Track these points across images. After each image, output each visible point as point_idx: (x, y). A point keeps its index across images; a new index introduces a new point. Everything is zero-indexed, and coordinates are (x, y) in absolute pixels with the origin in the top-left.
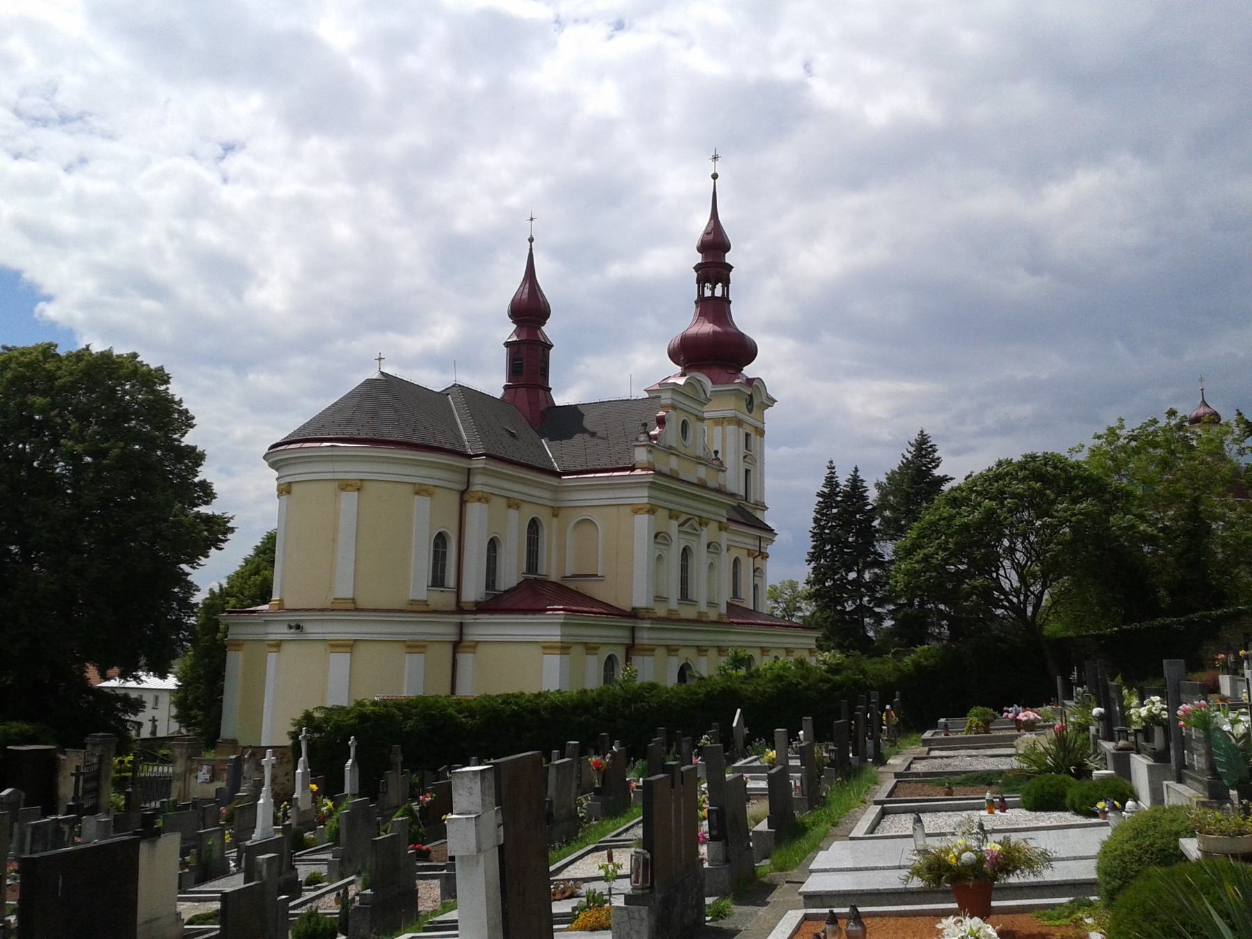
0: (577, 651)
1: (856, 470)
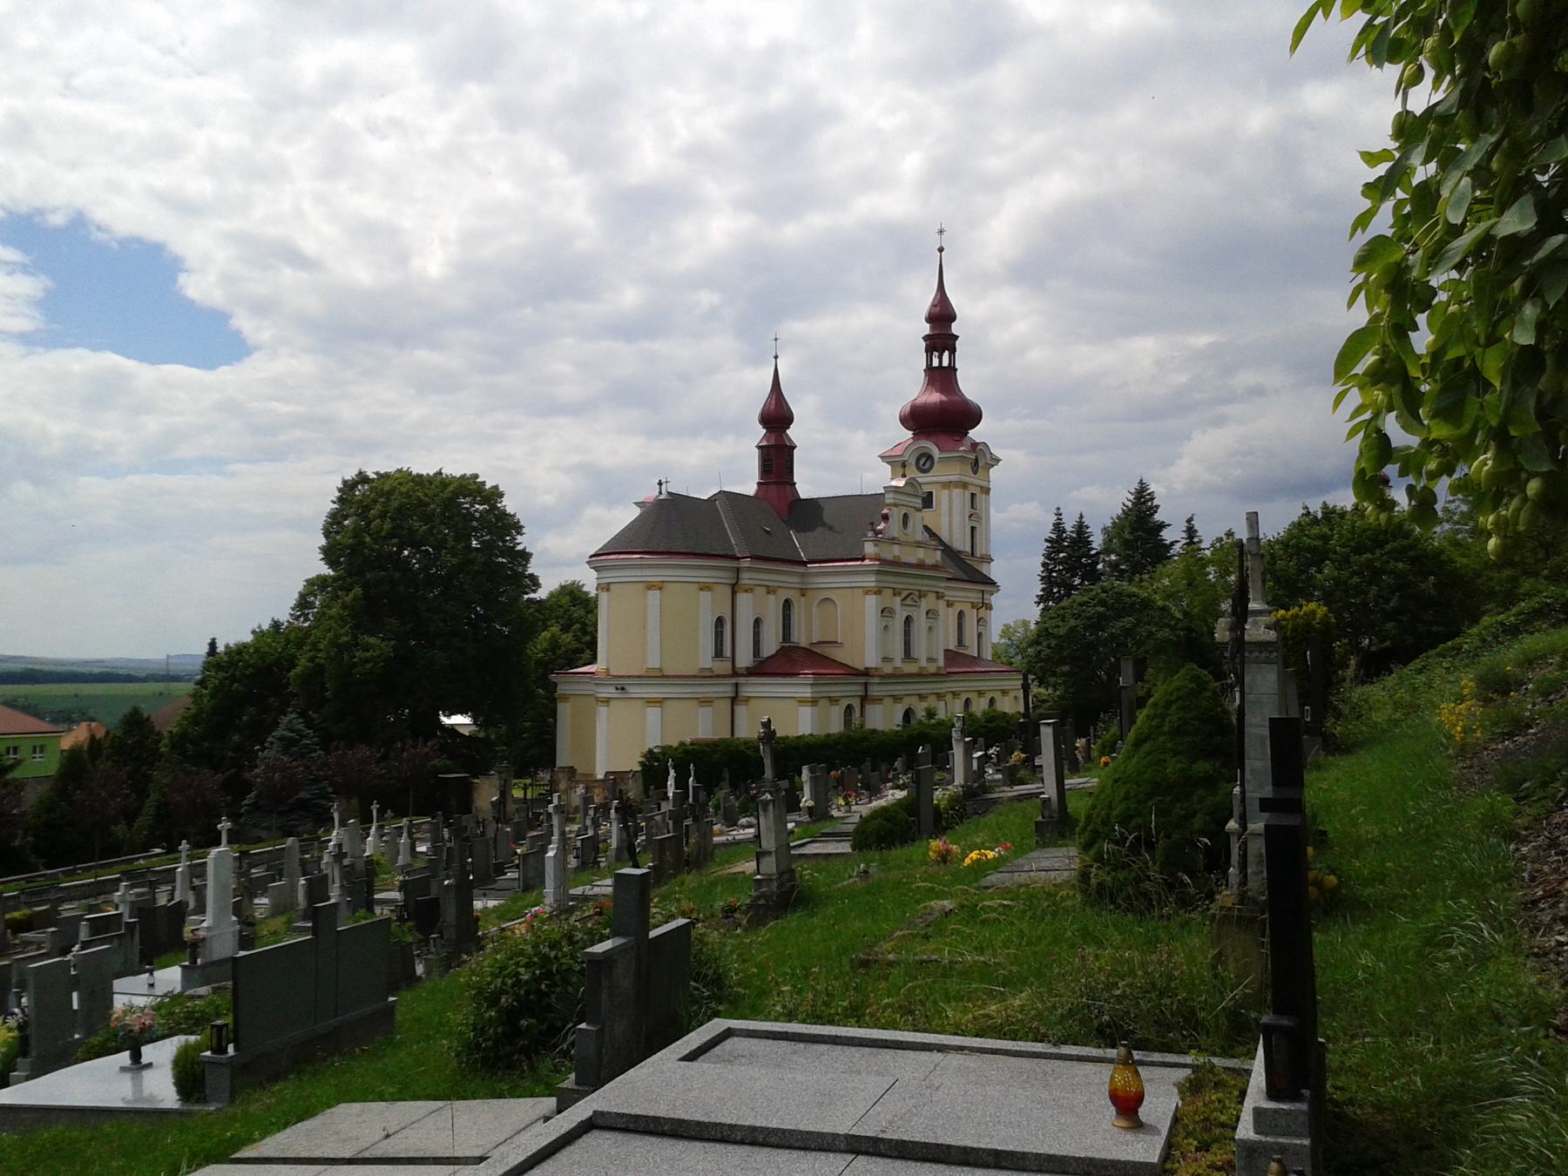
0: (823, 703)
1: (1081, 517)
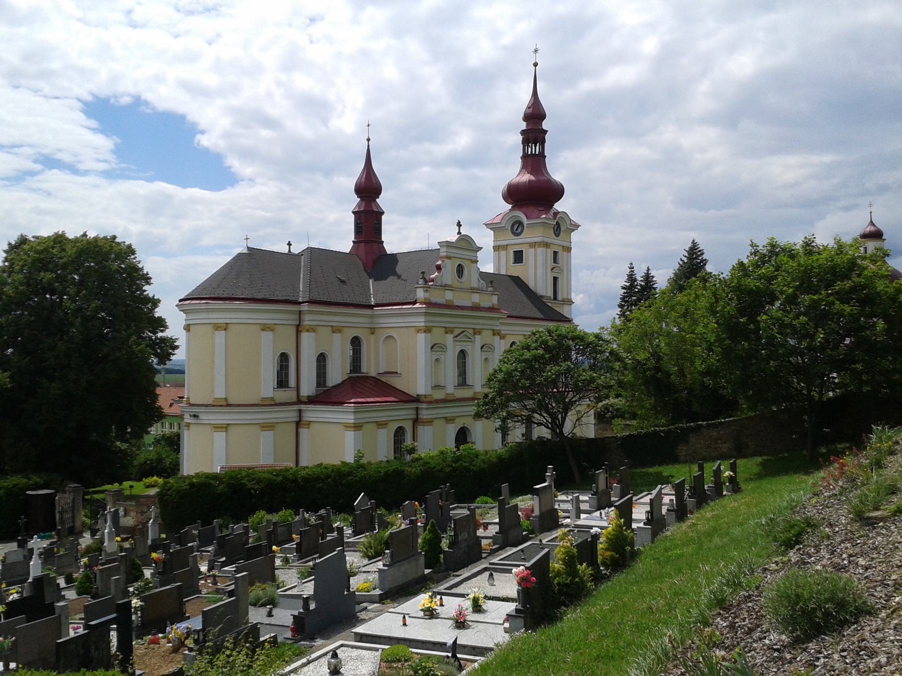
1: (648, 270)
